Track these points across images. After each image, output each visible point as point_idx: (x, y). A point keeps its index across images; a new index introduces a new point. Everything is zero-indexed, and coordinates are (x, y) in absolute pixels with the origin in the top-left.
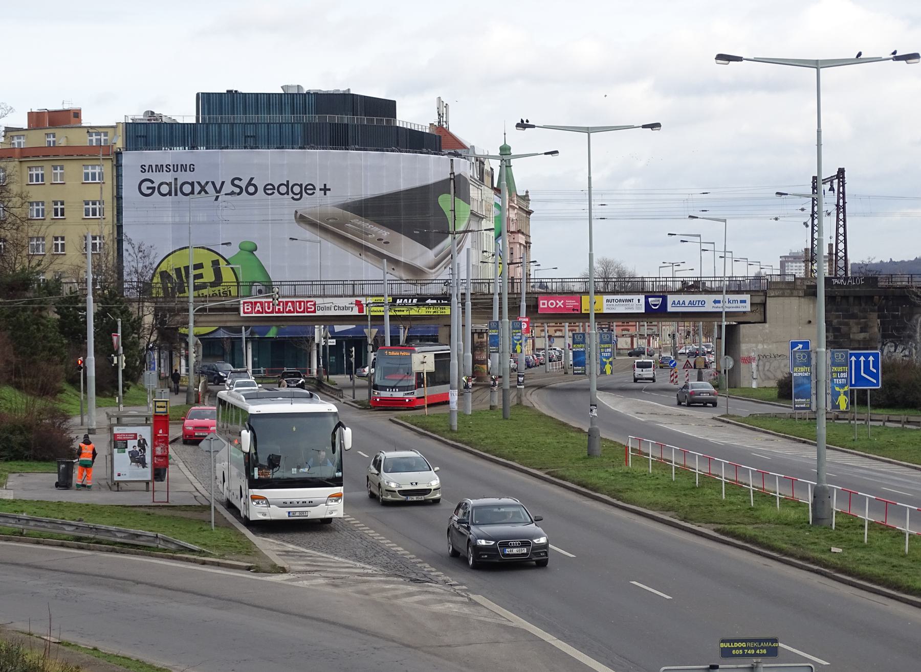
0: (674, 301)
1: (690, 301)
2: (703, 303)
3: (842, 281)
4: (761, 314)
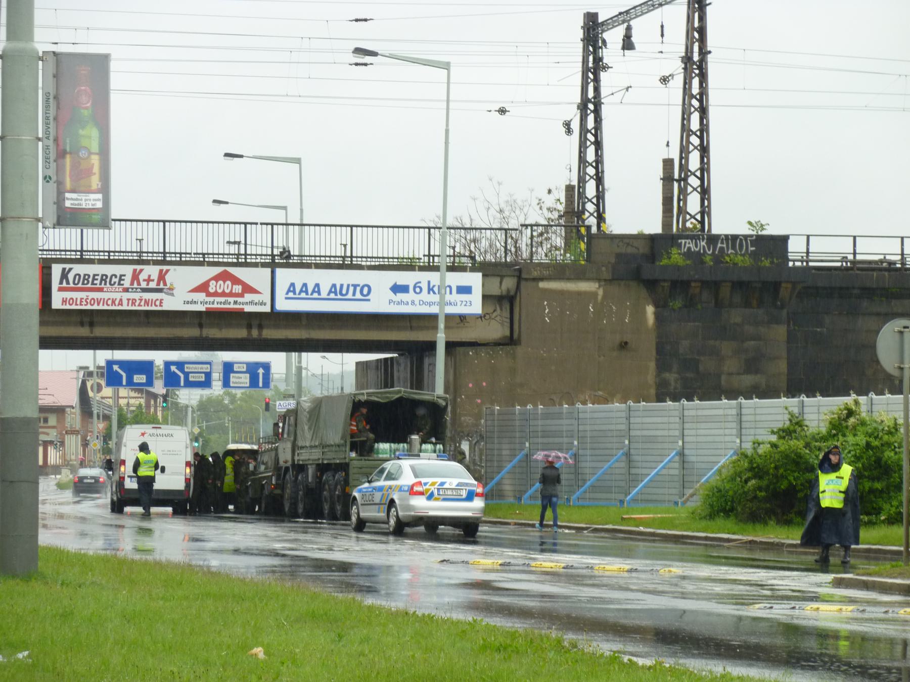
0: (293, 285)
1: (334, 286)
2: (366, 291)
3: (703, 243)
4: (502, 324)
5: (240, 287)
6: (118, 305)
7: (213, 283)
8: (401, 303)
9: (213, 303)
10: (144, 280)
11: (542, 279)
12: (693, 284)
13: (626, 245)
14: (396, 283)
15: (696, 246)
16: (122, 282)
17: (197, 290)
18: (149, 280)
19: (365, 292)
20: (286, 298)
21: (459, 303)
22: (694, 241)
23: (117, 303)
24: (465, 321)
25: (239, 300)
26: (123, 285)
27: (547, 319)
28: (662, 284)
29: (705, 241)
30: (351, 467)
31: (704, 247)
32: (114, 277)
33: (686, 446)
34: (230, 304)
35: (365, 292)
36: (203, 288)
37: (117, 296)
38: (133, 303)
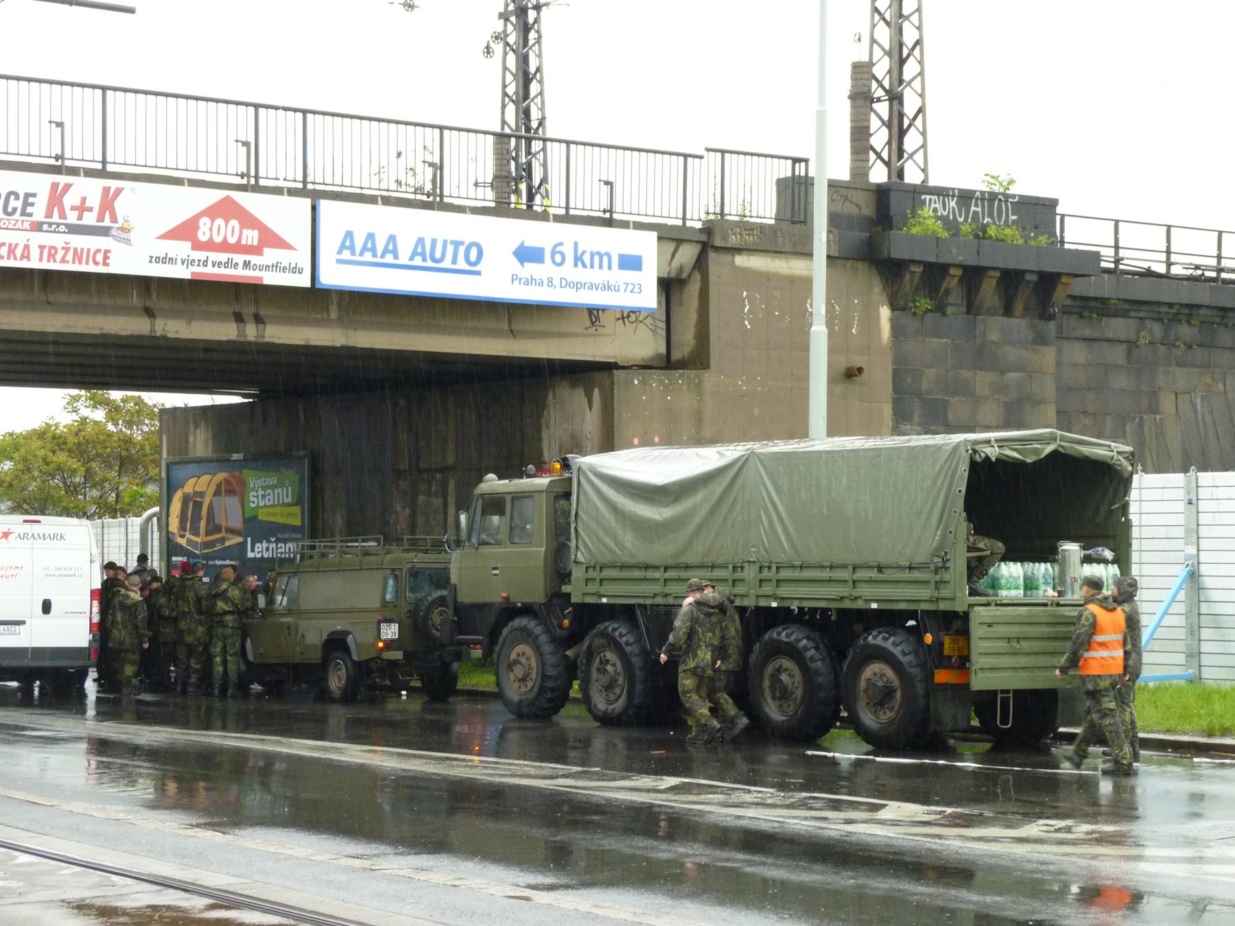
0: (349, 234)
1: (421, 241)
2: (474, 256)
3: (953, 204)
4: (654, 332)
5: (256, 233)
6: (21, 259)
7: (205, 222)
8: (530, 281)
9: (205, 264)
10: (73, 208)
11: (738, 250)
12: (952, 271)
13: (843, 199)
14: (523, 243)
15: (944, 209)
16: (29, 210)
17: (172, 235)
18: (82, 209)
19: (473, 257)
20: (339, 261)
21: (623, 287)
22: (941, 198)
23: (19, 252)
24: (597, 323)
25: (254, 259)
26: (31, 215)
27: (746, 323)
28: (913, 268)
30: (974, 625)
31: (953, 209)
32: (12, 197)
33: (1204, 557)
34: (236, 269)
35: (473, 257)
36: (186, 231)
37: (19, 238)
38: (50, 255)
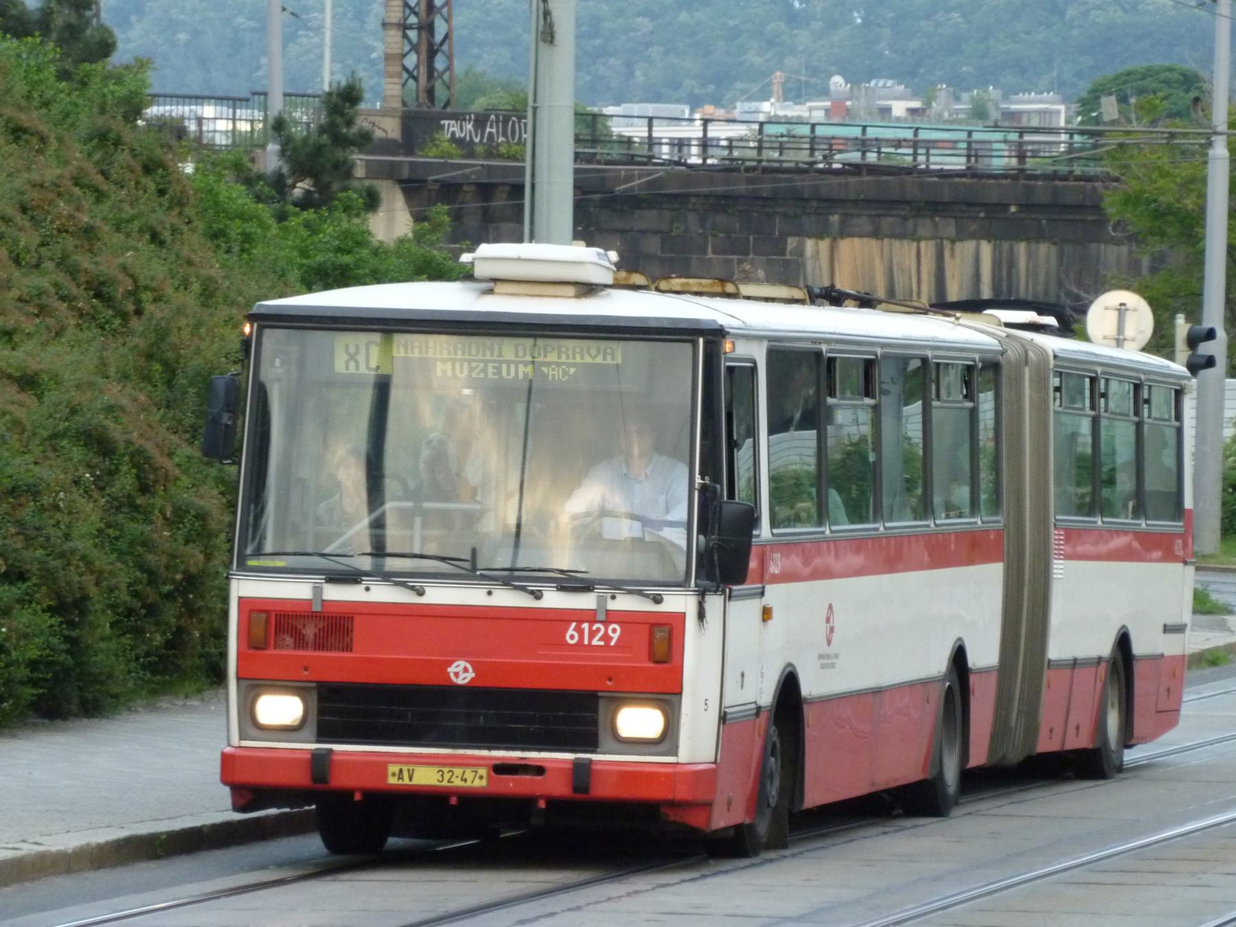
3: (470, 126)
12: (465, 188)
29: (472, 123)
31: (470, 132)
